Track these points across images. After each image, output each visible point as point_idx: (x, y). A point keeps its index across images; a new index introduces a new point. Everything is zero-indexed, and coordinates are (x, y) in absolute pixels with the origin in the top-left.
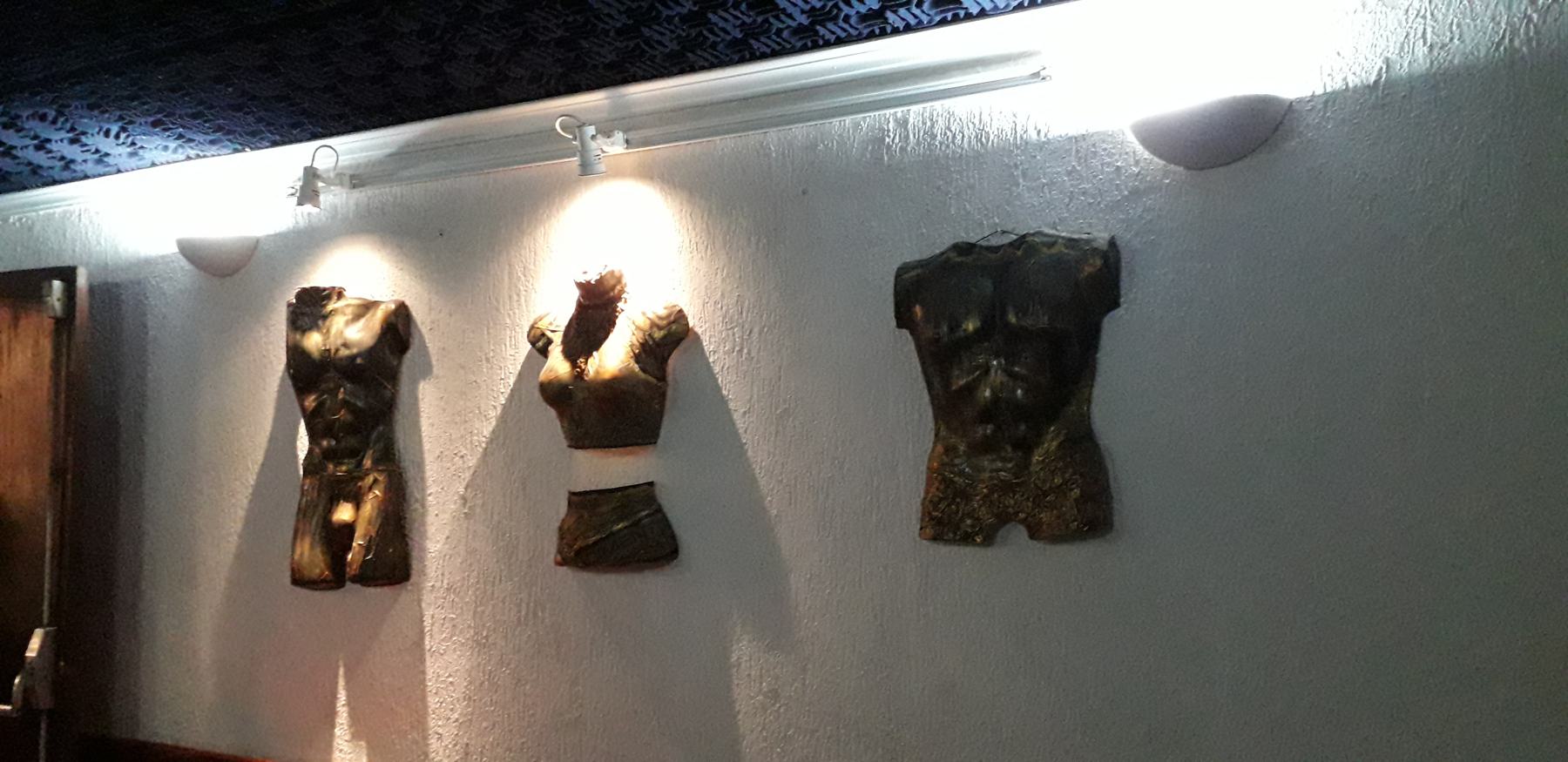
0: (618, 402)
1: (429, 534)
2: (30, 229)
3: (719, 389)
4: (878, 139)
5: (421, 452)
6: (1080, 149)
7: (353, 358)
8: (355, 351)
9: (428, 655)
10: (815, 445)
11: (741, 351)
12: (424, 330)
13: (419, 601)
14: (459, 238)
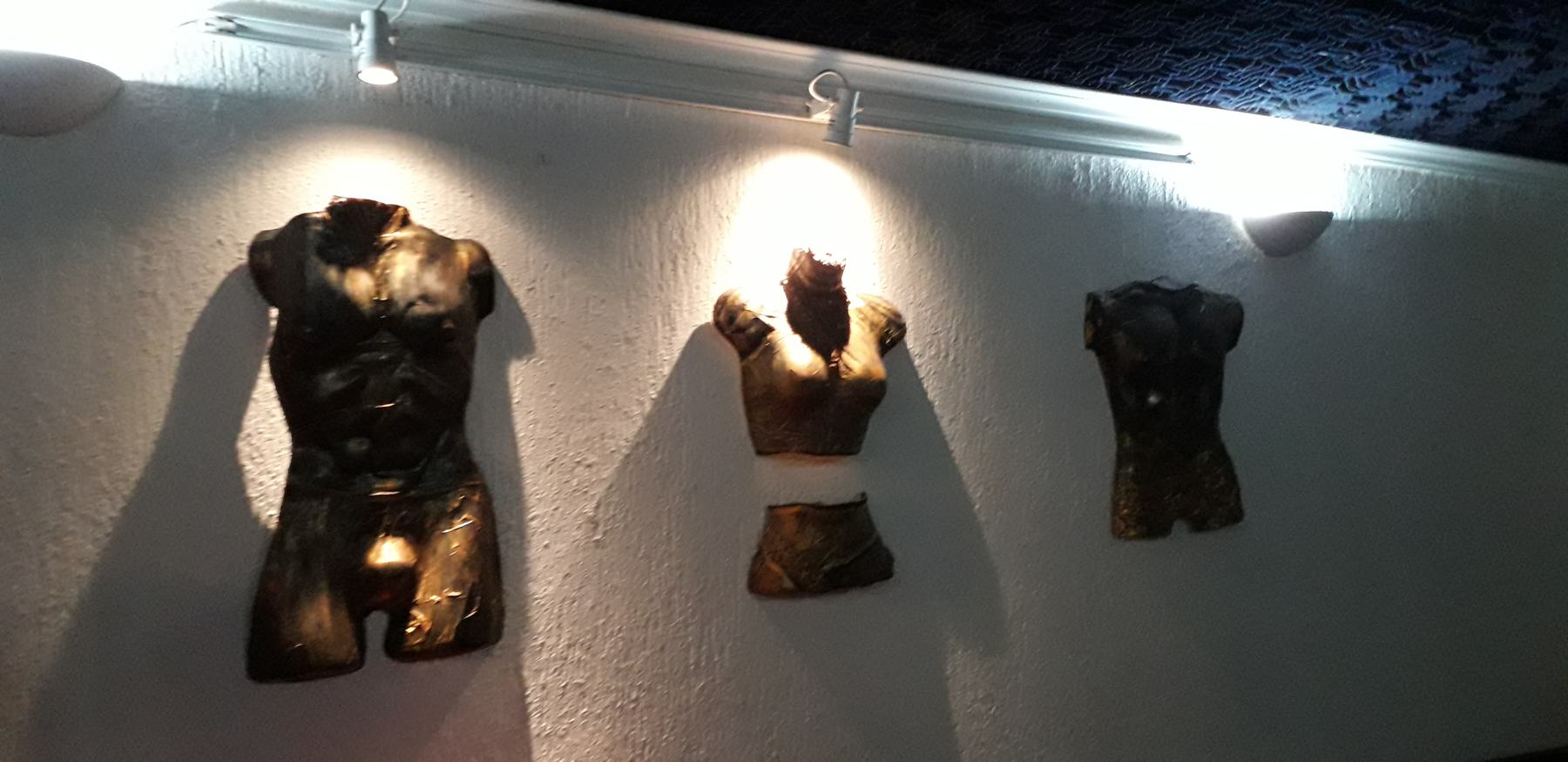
0: (798, 402)
1: (533, 574)
2: (429, 102)
3: (925, 394)
4: (1067, 175)
5: (516, 460)
6: (1205, 223)
7: (437, 319)
8: (441, 308)
9: (535, 743)
10: (1006, 454)
11: (947, 356)
12: (519, 292)
13: (518, 669)
14: (606, 183)
